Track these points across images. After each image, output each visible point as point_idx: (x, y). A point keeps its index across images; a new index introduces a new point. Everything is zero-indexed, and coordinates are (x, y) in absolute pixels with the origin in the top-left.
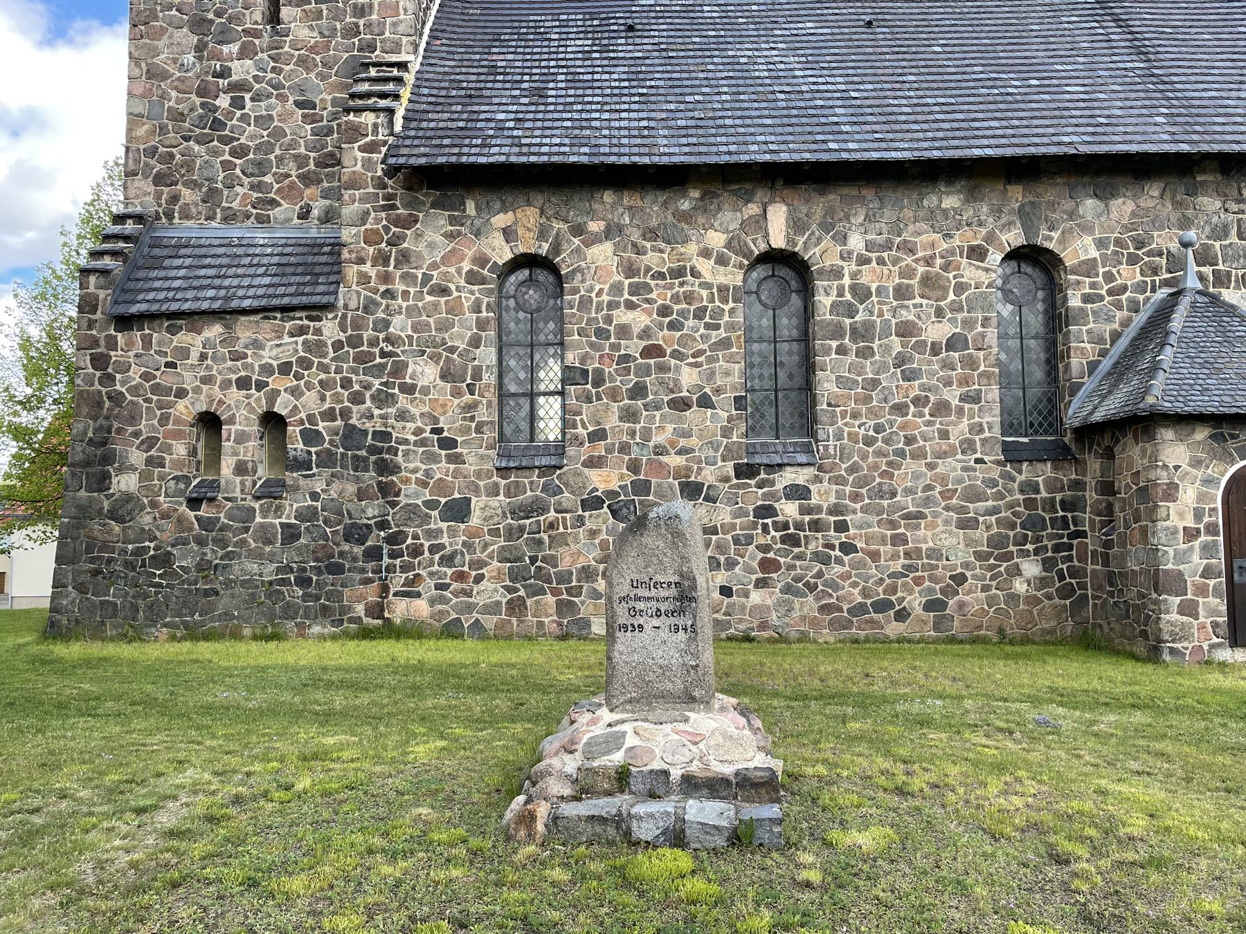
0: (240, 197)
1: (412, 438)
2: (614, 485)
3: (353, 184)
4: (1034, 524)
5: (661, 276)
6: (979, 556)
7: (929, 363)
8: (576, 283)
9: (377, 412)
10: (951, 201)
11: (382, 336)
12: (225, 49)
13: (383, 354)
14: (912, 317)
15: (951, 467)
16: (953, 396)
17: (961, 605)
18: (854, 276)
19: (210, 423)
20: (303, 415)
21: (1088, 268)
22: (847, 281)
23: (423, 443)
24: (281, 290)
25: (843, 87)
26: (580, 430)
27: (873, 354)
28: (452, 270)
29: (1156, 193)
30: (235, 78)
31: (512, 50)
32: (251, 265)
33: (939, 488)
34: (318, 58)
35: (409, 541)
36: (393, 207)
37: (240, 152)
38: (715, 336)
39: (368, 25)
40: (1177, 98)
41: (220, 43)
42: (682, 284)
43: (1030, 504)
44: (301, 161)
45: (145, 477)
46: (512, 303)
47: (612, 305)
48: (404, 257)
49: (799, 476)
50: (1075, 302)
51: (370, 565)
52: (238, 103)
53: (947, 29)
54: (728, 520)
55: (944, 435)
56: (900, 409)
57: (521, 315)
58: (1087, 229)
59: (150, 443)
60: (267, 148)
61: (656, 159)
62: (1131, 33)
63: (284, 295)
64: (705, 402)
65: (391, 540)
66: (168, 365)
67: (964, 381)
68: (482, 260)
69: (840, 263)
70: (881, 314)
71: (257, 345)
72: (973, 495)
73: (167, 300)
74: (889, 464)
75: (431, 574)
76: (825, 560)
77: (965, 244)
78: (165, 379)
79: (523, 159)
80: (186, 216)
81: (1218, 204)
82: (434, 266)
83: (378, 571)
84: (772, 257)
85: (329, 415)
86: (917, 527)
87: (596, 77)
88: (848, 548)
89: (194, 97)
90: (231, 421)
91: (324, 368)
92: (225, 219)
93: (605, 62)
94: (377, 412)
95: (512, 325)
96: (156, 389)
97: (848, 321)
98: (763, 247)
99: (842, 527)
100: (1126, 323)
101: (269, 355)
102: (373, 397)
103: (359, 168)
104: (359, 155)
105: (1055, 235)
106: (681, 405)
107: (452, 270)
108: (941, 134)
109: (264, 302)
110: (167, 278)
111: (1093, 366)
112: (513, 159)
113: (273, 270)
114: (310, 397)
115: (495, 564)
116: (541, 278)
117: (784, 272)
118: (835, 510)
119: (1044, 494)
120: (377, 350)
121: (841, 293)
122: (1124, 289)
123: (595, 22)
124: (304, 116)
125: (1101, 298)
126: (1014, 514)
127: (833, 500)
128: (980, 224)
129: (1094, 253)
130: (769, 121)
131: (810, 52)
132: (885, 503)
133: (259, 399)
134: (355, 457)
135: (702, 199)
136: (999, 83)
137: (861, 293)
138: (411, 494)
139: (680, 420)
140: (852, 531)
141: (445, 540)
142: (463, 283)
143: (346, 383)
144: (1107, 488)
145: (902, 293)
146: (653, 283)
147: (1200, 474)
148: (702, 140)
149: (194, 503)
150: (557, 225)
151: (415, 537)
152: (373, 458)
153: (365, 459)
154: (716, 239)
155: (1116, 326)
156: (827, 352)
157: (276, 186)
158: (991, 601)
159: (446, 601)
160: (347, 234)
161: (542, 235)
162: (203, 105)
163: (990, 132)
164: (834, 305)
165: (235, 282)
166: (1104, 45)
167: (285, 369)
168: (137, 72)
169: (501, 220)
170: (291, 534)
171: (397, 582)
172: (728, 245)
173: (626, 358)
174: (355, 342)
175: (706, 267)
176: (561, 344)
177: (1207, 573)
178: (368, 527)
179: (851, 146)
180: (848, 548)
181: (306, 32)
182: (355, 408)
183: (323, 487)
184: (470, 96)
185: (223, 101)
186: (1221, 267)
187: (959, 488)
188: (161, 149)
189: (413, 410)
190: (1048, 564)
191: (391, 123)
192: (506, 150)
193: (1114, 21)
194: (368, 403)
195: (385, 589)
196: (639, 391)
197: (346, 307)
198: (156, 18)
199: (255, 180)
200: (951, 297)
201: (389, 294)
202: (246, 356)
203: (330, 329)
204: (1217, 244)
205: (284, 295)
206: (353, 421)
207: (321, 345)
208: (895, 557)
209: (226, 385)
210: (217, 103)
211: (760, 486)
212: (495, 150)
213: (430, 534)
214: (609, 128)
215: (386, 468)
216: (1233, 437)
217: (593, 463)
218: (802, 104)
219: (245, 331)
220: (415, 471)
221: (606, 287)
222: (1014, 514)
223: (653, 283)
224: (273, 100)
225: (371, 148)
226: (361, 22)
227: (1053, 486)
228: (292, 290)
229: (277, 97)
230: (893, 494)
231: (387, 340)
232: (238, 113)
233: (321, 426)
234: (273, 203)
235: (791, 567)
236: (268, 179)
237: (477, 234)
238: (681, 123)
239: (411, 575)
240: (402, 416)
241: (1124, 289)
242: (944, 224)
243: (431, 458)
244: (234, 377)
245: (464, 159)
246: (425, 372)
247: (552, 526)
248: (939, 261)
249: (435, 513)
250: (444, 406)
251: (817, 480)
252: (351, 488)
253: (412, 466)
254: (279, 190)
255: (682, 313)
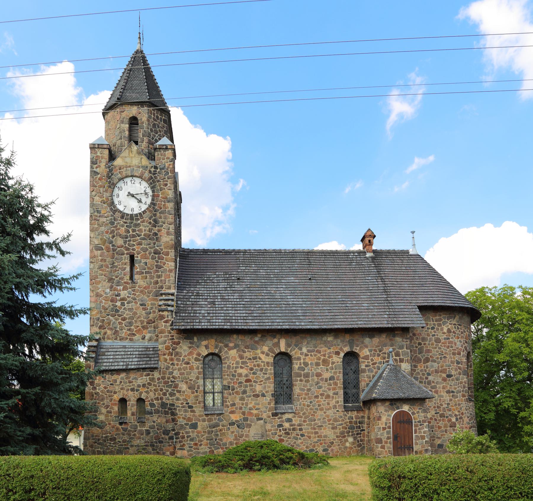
0: (124, 333)
1: (181, 406)
2: (238, 419)
3: (162, 332)
4: (352, 428)
5: (250, 359)
6: (337, 437)
7: (325, 384)
8: (226, 361)
9: (170, 398)
10: (330, 339)
11: (171, 376)
12: (119, 288)
13: (172, 382)
14: (320, 371)
15: (330, 413)
16: (331, 393)
17: (332, 450)
18: (304, 359)
19: (123, 401)
20: (149, 399)
21: (366, 358)
22: (302, 361)
23: (183, 407)
24: (141, 363)
25: (301, 303)
26: (228, 403)
27: (309, 381)
28: (190, 357)
29: (384, 337)
30: (122, 296)
31: (203, 286)
32: (130, 354)
33: (327, 419)
34: (146, 291)
35: (181, 434)
36: (173, 339)
37: (124, 319)
38: (266, 376)
39: (161, 281)
40: (392, 309)
41: (117, 286)
42: (256, 361)
43: (351, 422)
44: (142, 322)
45: (106, 416)
46: (207, 366)
47: (237, 367)
48: (177, 354)
49: (290, 416)
50: (363, 366)
51: (170, 441)
52: (123, 304)
53: (332, 281)
54: (270, 428)
55: (328, 404)
56: (317, 397)
57: (210, 369)
58: (366, 347)
59: (107, 407)
60: (132, 318)
61: (248, 327)
62: (385, 284)
63: (142, 365)
64: (263, 395)
65: (176, 434)
66: (111, 384)
67: (334, 389)
68: (199, 354)
69: (300, 356)
70: (311, 370)
71: (136, 379)
72: (336, 420)
73: (109, 366)
74: (314, 412)
75: (188, 444)
76: (297, 439)
77: (334, 353)
78: (110, 388)
79: (211, 327)
80: (109, 338)
81: (401, 340)
82: (185, 356)
83: (172, 443)
84: (281, 353)
85: (157, 399)
86: (321, 429)
87: (229, 297)
88: (302, 435)
89: (109, 302)
90: (130, 400)
91: (155, 385)
92: (120, 340)
93: (232, 292)
94: (170, 398)
95: (207, 373)
96: (108, 391)
97: (302, 372)
98: (279, 351)
99: (301, 430)
100: (376, 373)
101: (140, 381)
102: (169, 394)
103: (163, 328)
104: (164, 324)
105: (358, 348)
106: (257, 396)
107: (190, 357)
108: (327, 320)
109: (138, 367)
110: (108, 359)
111: (368, 385)
112: (209, 327)
113: (138, 356)
114: (152, 394)
115: (205, 441)
116: (215, 359)
117: (284, 357)
118: (300, 425)
119: (354, 420)
120: (170, 380)
121: (300, 365)
122: (376, 363)
123: (227, 276)
124: (143, 308)
125: (370, 366)
126: (347, 425)
127: (299, 422)
128: (338, 345)
129: (368, 353)
130: (280, 315)
131: (292, 289)
132: (313, 423)
133: (137, 394)
134: (165, 411)
135: (261, 337)
136: (345, 302)
137: (306, 364)
138: (181, 421)
139: (257, 400)
140: (304, 431)
141: (191, 434)
142: (194, 361)
143: (161, 390)
144: (369, 418)
145: (317, 364)
146: (248, 361)
147: (387, 414)
148: (261, 321)
149: (121, 424)
150: (220, 345)
151: (183, 433)
152: (170, 411)
153: (168, 412)
154: (266, 349)
155: (374, 374)
156: (297, 381)
157: (135, 330)
158: (340, 449)
159: (192, 451)
160: (160, 347)
161: (216, 347)
162: (112, 305)
163: (340, 320)
164: (299, 368)
165: (128, 360)
166: (376, 288)
167: (144, 386)
168: (92, 295)
169: (204, 343)
170: (148, 432)
171: (178, 446)
172: (269, 350)
173: (241, 383)
174: (163, 378)
175: (263, 357)
176: (222, 378)
177: (388, 438)
178: (169, 430)
179: (303, 324)
180: (302, 435)
181: (143, 283)
182: (164, 397)
183: (157, 420)
184: (193, 304)
185: (118, 304)
186: (401, 357)
187: (332, 418)
188: (101, 318)
189: (181, 398)
190: (355, 438)
191: (172, 314)
192: (206, 324)
193: (381, 279)
194: (168, 396)
195: (175, 448)
196: (244, 392)
197: (160, 368)
198: (98, 278)
199: (129, 328)
200: (330, 365)
201: (173, 364)
202: (133, 382)
203: (156, 375)
204: (400, 351)
205: (142, 365)
206: (164, 401)
207: (153, 379)
208: (315, 437)
209: (128, 390)
210: (117, 304)
211: (279, 419)
212: (203, 324)
213: (187, 433)
214: (235, 316)
215: (173, 414)
216: (395, 404)
217: (232, 412)
218: (289, 309)
219: (132, 375)
220: (182, 415)
221: (235, 362)
222: (347, 425)
223: (248, 361)
224: (133, 304)
225: (166, 322)
226: (159, 280)
227: (357, 417)
228: (144, 363)
229: (135, 302)
230: (315, 420)
231: (173, 377)
232: (123, 307)
233: (155, 402)
234: (134, 335)
235: (287, 441)
236: (132, 327)
237: (198, 347)
238: (255, 315)
239: (182, 444)
240: (178, 399)
241: (376, 363)
242: (329, 345)
243: (186, 411)
244: (130, 388)
245: (195, 327)
246: (183, 387)
247: (221, 430)
248: (327, 355)
249: (188, 427)
250: (189, 396)
251: (294, 417)
252: (164, 420)
253: (181, 413)
254: (136, 331)
255: (256, 370)
